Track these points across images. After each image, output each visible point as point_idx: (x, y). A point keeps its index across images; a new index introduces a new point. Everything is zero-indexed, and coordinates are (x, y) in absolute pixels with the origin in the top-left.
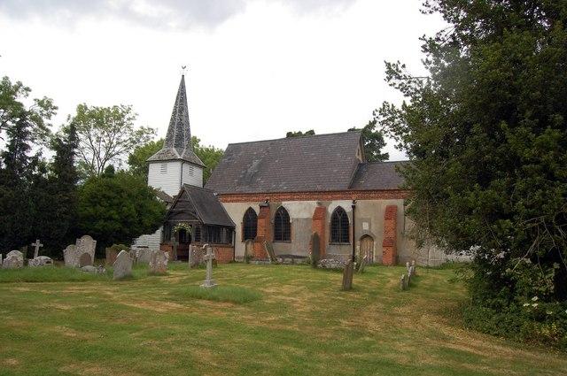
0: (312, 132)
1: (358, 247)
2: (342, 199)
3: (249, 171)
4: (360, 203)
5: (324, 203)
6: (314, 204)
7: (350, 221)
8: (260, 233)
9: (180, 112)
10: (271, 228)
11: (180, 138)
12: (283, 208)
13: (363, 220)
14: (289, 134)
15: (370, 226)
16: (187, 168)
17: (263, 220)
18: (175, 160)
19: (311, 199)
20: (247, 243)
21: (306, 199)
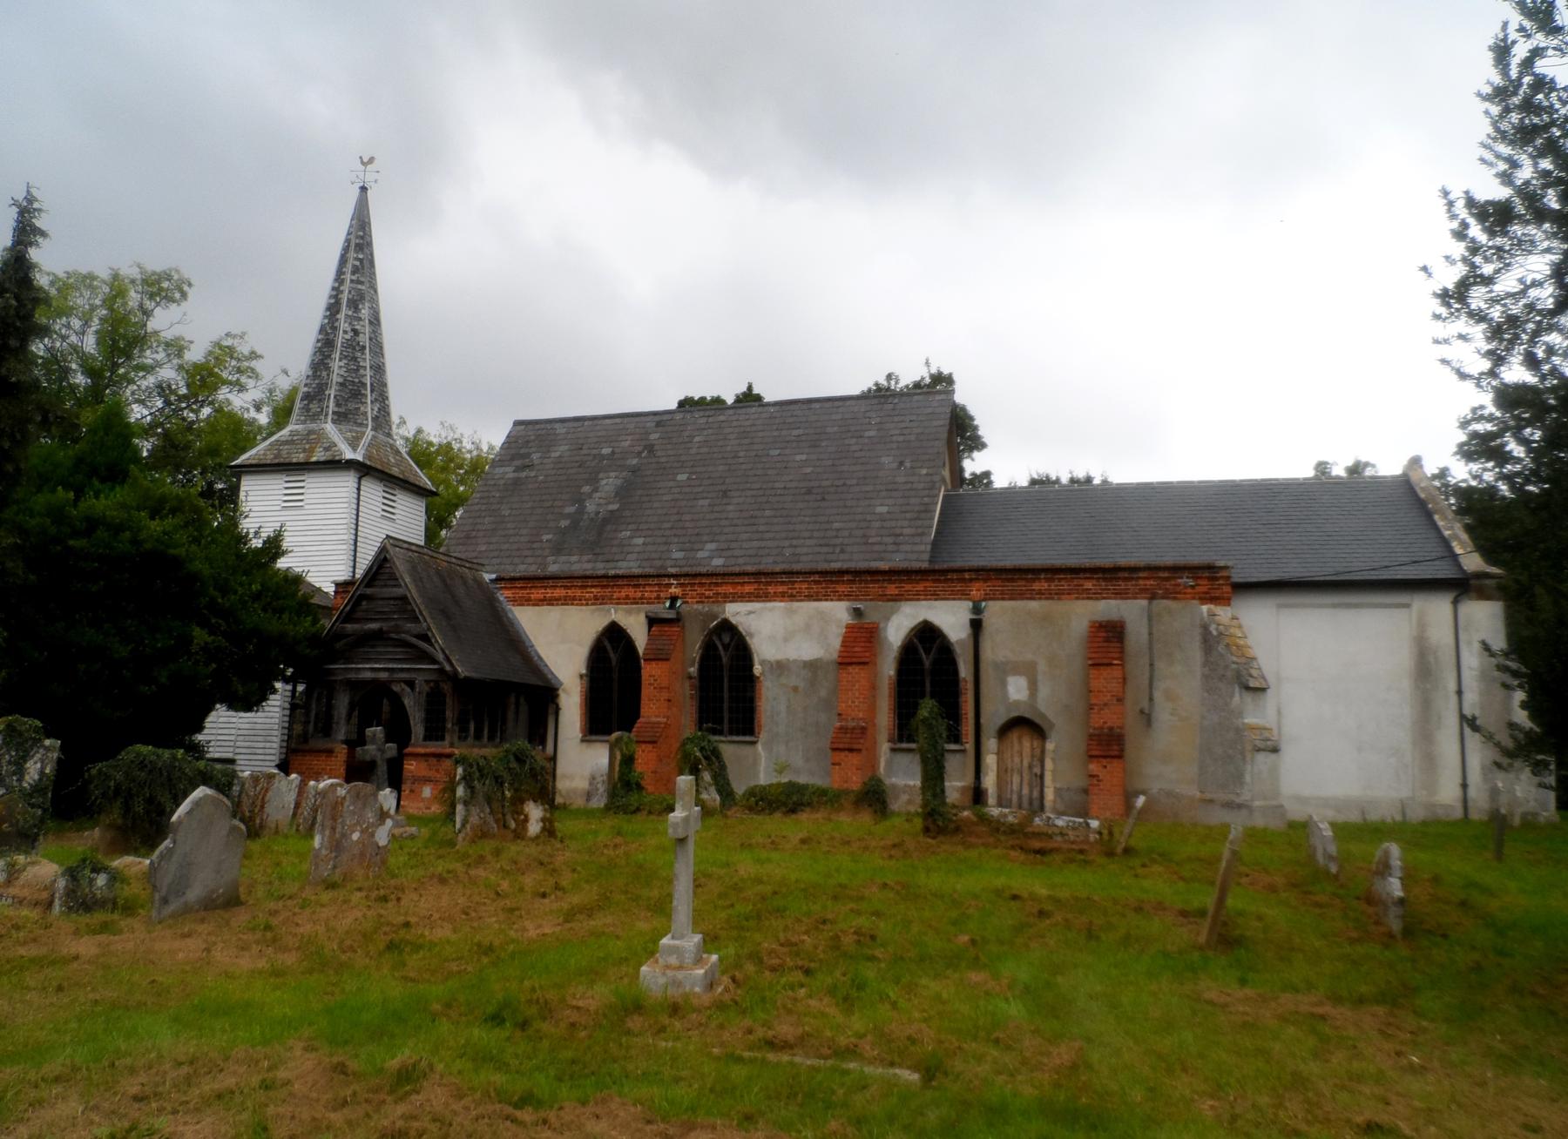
0: (749, 398)
1: (990, 760)
2: (936, 596)
3: (590, 507)
4: (998, 613)
5: (873, 611)
6: (838, 612)
7: (965, 671)
8: (652, 710)
9: (354, 304)
10: (686, 694)
11: (352, 392)
12: (727, 627)
13: (1006, 669)
14: (682, 404)
15: (1033, 686)
16: (373, 492)
17: (664, 666)
18: (335, 465)
19: (826, 598)
20: (1562, 254)
21: (810, 598)
